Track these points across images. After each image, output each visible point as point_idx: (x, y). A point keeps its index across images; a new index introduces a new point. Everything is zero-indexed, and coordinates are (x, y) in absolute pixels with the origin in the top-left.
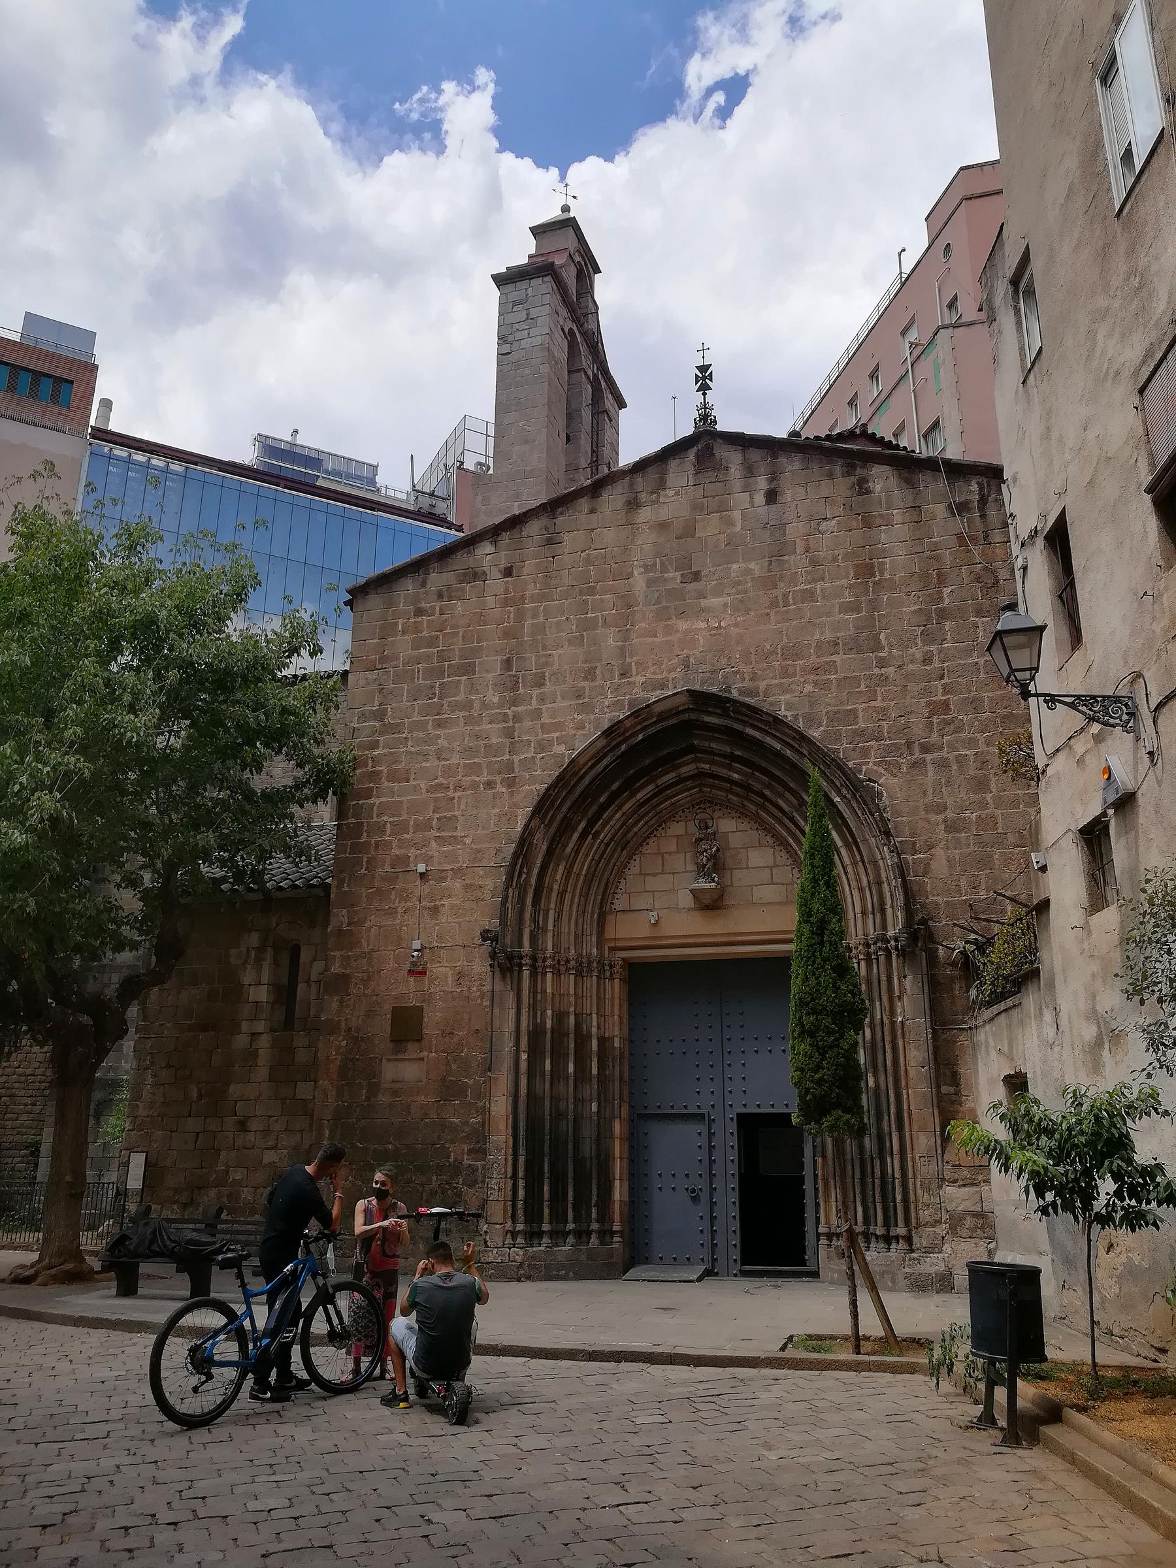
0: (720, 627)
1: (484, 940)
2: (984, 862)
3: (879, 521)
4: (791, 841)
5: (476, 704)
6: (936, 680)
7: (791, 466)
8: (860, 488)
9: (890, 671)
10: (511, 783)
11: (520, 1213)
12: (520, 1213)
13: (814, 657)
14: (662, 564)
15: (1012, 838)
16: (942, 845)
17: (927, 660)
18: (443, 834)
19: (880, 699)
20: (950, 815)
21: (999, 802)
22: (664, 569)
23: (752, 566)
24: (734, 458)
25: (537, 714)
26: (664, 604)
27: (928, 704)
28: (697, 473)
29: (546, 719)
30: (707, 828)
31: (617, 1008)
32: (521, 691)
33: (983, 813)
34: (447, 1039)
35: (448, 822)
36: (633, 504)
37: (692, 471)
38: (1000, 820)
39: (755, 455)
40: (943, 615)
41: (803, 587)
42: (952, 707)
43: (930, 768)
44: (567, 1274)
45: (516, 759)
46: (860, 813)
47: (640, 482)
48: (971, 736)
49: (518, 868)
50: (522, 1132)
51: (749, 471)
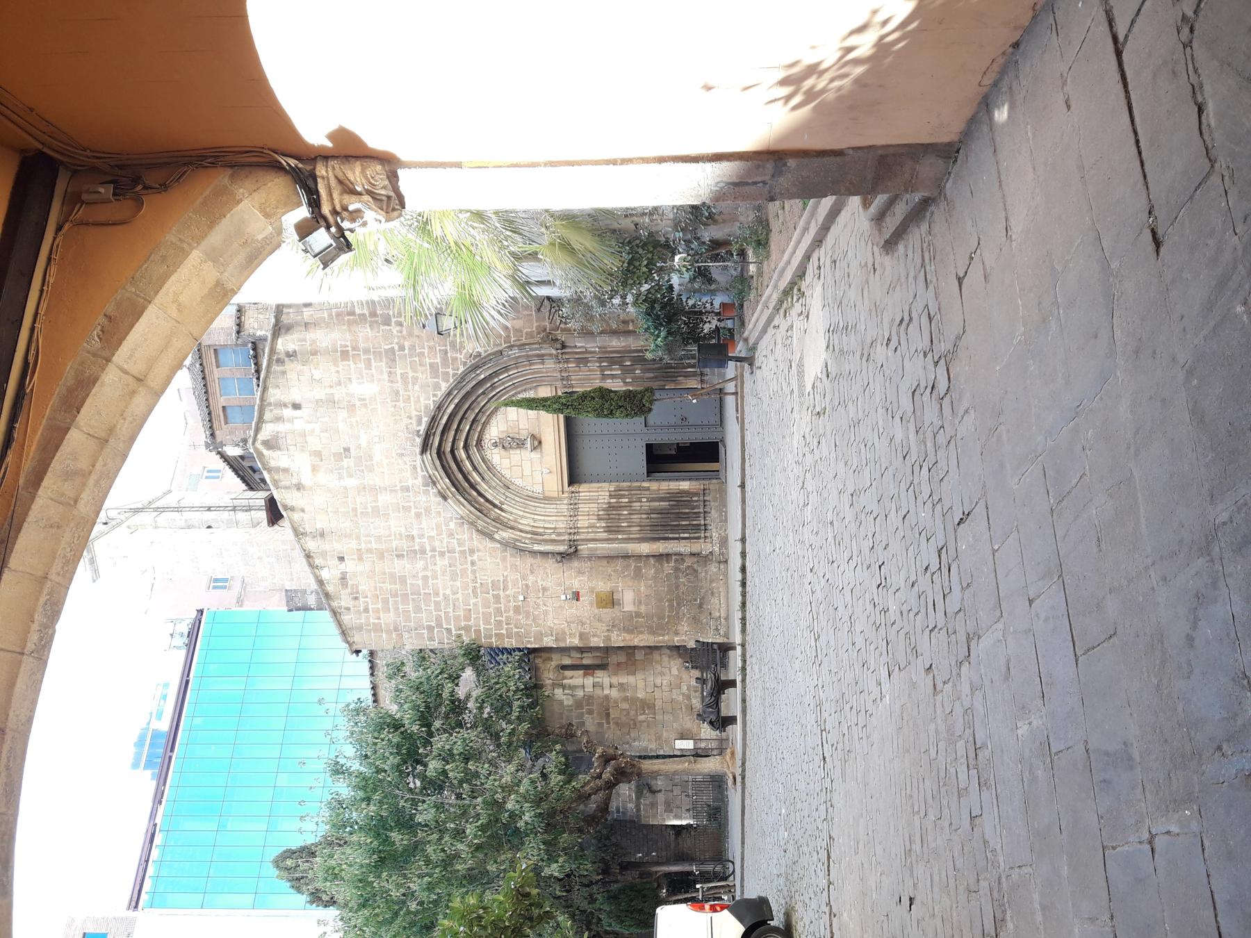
9: (407, 344)
29: (434, 534)
37: (278, 452)
45: (458, 549)
51: (279, 419)
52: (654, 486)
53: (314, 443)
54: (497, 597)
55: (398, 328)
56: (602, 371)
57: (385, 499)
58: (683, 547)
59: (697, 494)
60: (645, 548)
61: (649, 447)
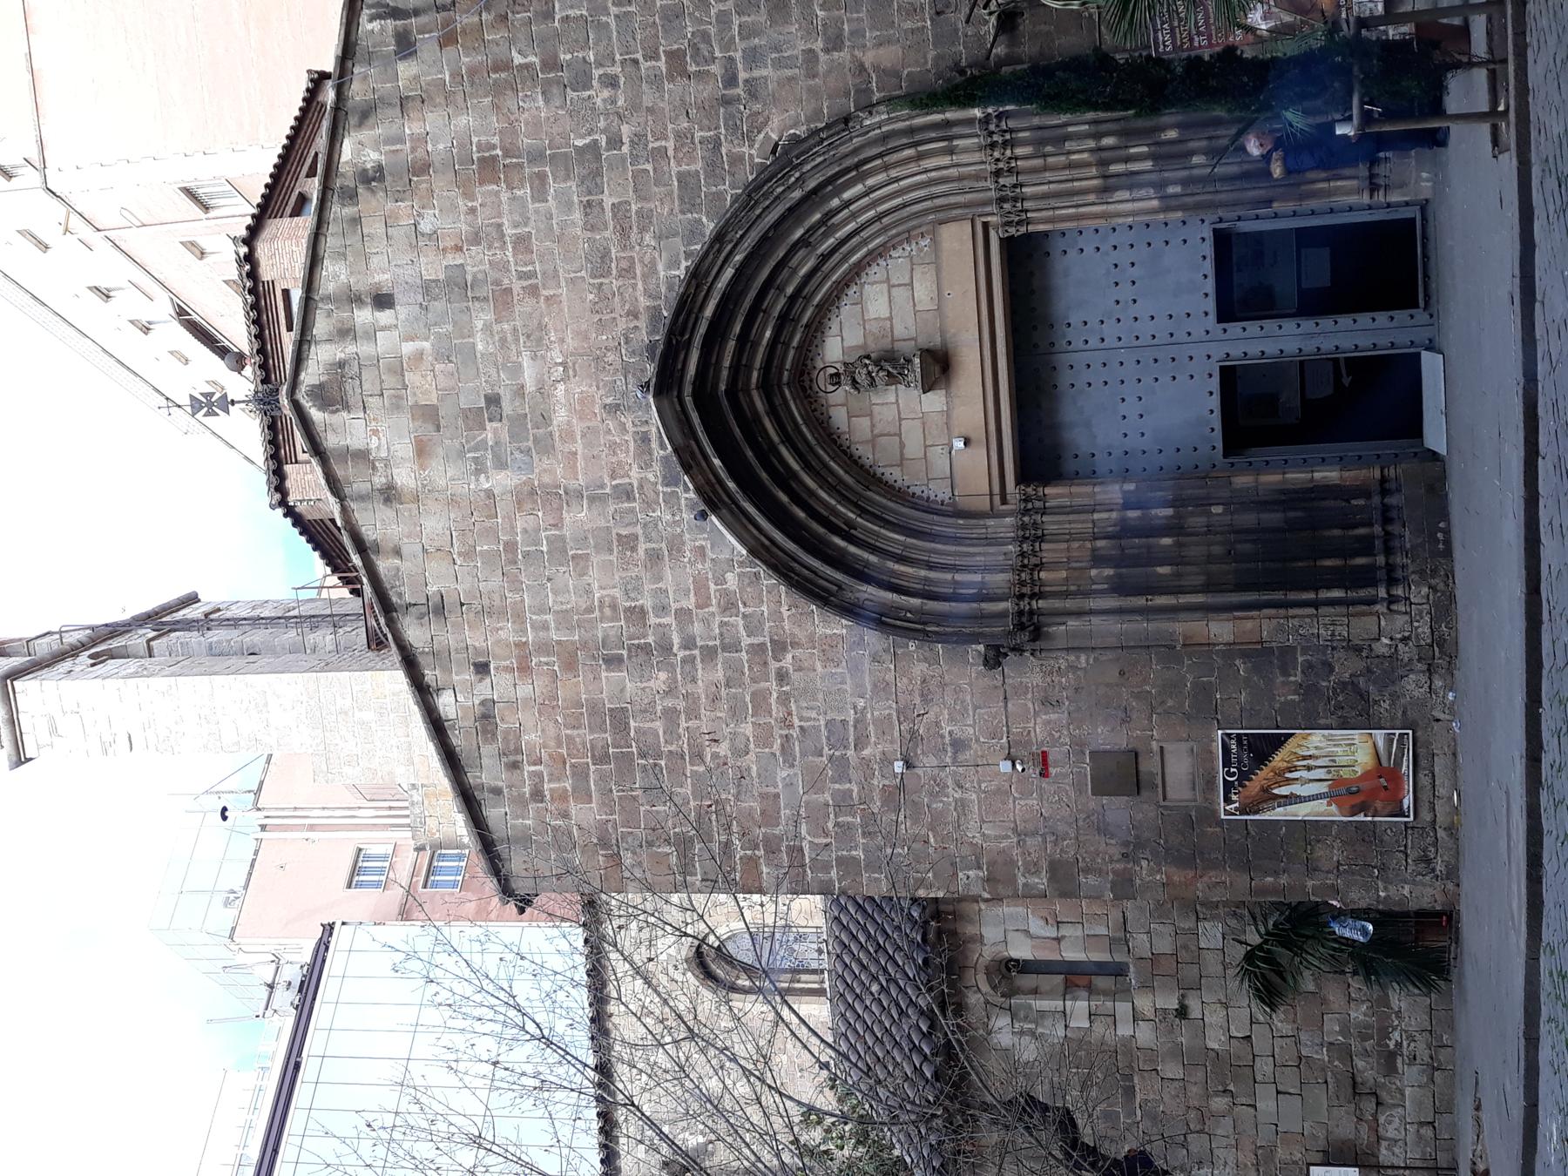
3: (420, 153)
5: (669, 703)
9: (626, 130)
13: (607, 234)
14: (476, 449)
17: (611, 82)
18: (851, 739)
20: (819, 45)
22: (482, 446)
25: (683, 615)
26: (530, 444)
27: (671, 79)
29: (690, 602)
30: (837, 375)
32: (650, 640)
36: (389, 494)
40: (551, 64)
41: (509, 253)
43: (756, 73)
45: (746, 641)
51: (345, 333)
53: (423, 386)
55: (606, 93)
61: (1230, 376)
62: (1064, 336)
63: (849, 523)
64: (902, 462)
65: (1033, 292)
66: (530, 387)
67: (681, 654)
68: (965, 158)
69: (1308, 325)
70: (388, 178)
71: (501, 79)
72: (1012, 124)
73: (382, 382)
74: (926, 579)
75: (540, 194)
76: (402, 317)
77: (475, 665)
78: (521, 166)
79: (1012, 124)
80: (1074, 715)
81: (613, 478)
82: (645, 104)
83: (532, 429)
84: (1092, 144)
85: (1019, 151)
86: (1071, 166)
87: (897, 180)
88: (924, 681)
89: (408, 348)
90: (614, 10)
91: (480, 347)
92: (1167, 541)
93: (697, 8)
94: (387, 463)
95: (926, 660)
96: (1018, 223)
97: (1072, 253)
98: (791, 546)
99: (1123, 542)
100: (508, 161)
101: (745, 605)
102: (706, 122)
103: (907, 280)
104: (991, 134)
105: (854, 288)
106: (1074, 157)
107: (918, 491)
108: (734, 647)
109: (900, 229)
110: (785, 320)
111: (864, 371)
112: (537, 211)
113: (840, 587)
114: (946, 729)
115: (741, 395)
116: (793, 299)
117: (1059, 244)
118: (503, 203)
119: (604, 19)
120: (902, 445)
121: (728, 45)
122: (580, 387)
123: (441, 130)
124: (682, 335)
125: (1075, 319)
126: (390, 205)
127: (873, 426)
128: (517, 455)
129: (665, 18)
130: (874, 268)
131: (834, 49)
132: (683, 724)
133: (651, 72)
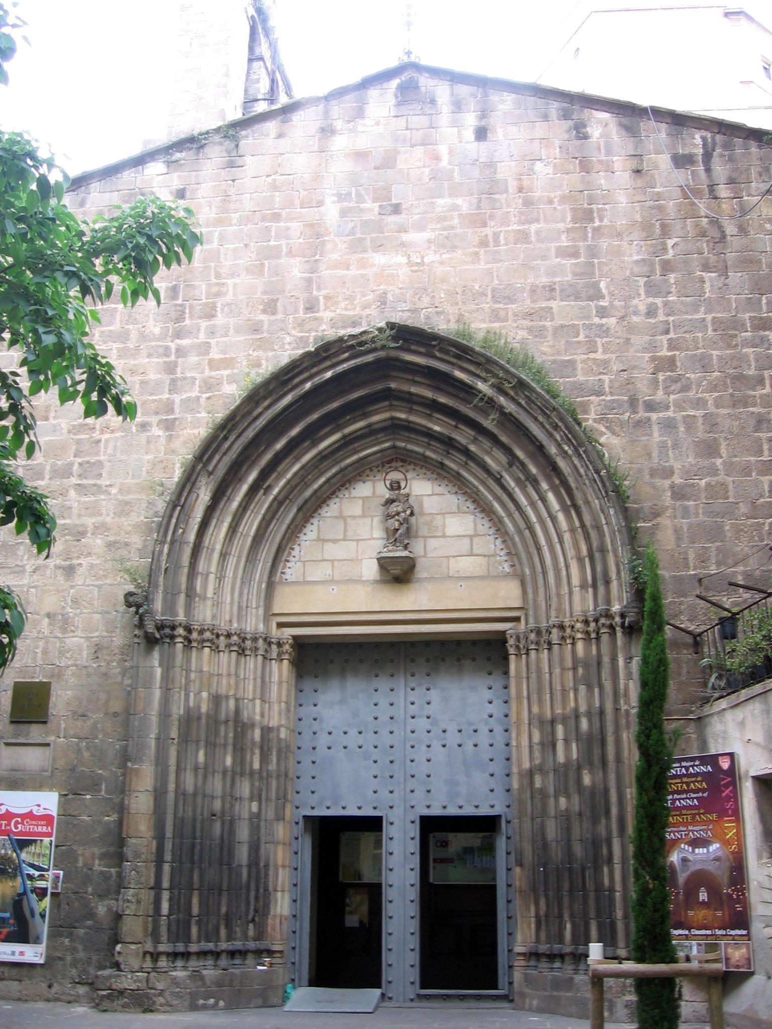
0: (422, 264)
1: (129, 605)
2: (716, 533)
3: (598, 167)
4: (496, 505)
5: (134, 335)
6: (662, 334)
7: (505, 103)
8: (578, 132)
9: (612, 321)
10: (169, 426)
11: (164, 931)
12: (164, 931)
13: (528, 302)
14: (358, 195)
15: (743, 508)
16: (669, 512)
17: (651, 312)
18: (85, 482)
19: (600, 350)
20: (677, 480)
21: (730, 467)
22: (360, 199)
23: (459, 201)
24: (443, 92)
25: (205, 348)
26: (359, 235)
27: (653, 359)
28: (399, 104)
29: (215, 354)
30: (399, 488)
31: (284, 693)
32: (187, 322)
33: (714, 480)
34: (79, 723)
35: (92, 468)
36: (327, 131)
37: (392, 101)
38: (731, 487)
39: (463, 90)
40: (667, 267)
41: (515, 227)
42: (679, 364)
43: (655, 428)
44: (216, 1003)
45: (177, 398)
46: (582, 471)
47: (337, 110)
48: (700, 395)
49: (174, 521)
50: (169, 833)
51: (458, 106)
52: (281, 831)
53: (412, 160)
54: (66, 472)
55: (642, 308)
56: (564, 720)
57: (296, 270)
58: (134, 902)
59: (260, 935)
60: (141, 802)
61: (374, 824)
62: (420, 685)
63: (269, 488)
64: (321, 540)
65: (459, 660)
66: (405, 237)
67: (173, 346)
68: (577, 598)
69: (414, 894)
70: (578, 143)
71: (656, 229)
72: (605, 638)
73: (417, 129)
74: (213, 550)
75: (563, 253)
76: (468, 146)
77: (184, 189)
78: (585, 239)
79: (605, 638)
80: (84, 672)
81: (326, 298)
82: (632, 337)
83: (370, 238)
84: (583, 709)
85: (580, 646)
86: (564, 691)
87: (561, 542)
88: (127, 544)
89: (443, 150)
90: (709, 317)
91: (440, 201)
92: (229, 761)
93: (710, 383)
94: (353, 131)
95: (145, 547)
96: (518, 647)
97: (488, 694)
98: (250, 433)
99: (231, 724)
100: (590, 230)
101: (209, 398)
102: (616, 385)
103: (476, 551)
104: (596, 621)
105: (472, 507)
106: (572, 695)
107: (295, 553)
108: (174, 387)
109: (519, 545)
110: (449, 443)
111: (400, 509)
112: (548, 249)
113: (210, 474)
114: (84, 561)
115: (387, 403)
116: (466, 452)
117: (496, 681)
118: (558, 223)
119: (702, 309)
120: (335, 541)
121: (679, 406)
122: (404, 273)
123: (616, 184)
124: (440, 350)
125: (434, 695)
126: (557, 143)
127: (354, 517)
128: (351, 225)
129: (703, 357)
130: (487, 525)
131: (673, 493)
132: (115, 346)
133: (658, 344)
